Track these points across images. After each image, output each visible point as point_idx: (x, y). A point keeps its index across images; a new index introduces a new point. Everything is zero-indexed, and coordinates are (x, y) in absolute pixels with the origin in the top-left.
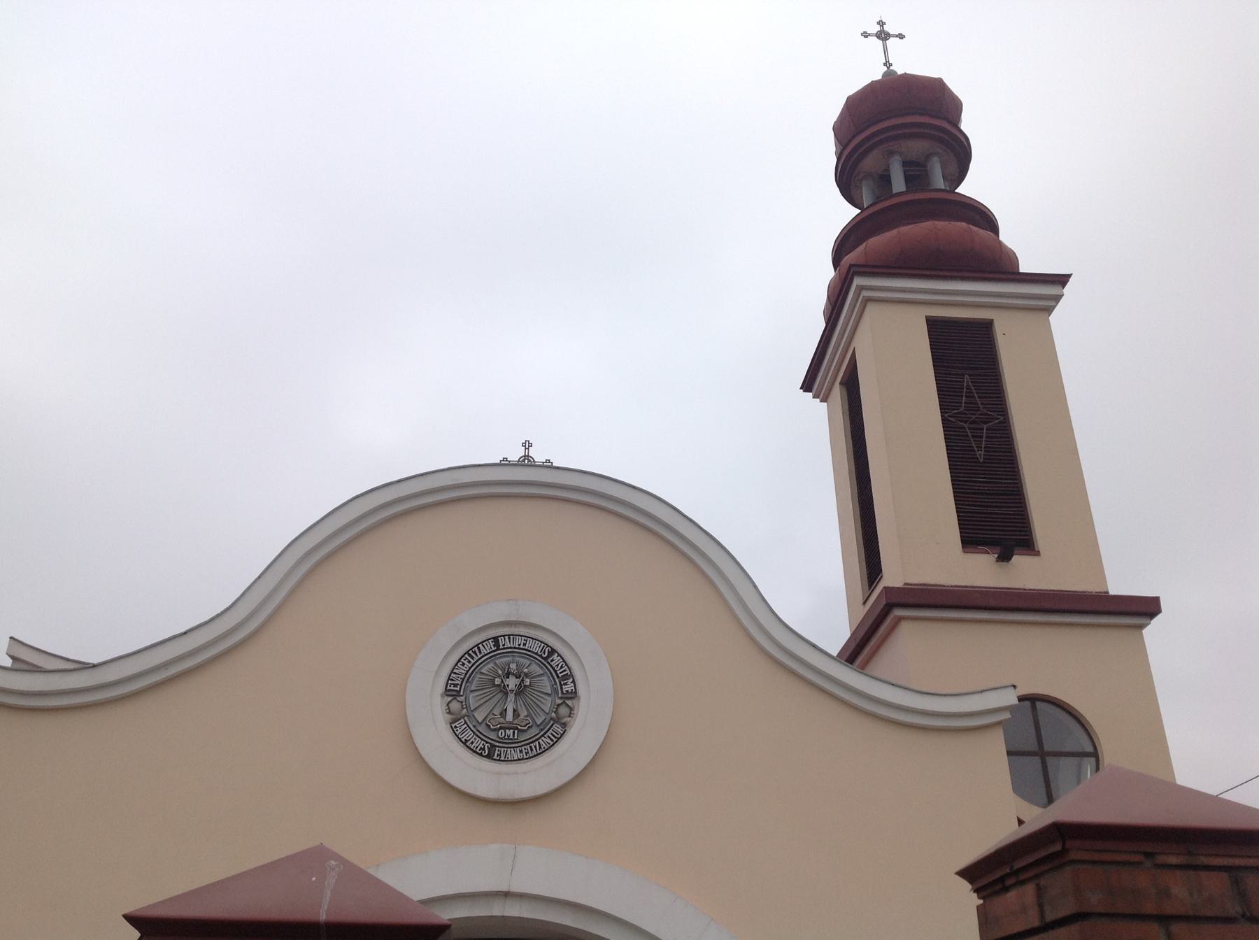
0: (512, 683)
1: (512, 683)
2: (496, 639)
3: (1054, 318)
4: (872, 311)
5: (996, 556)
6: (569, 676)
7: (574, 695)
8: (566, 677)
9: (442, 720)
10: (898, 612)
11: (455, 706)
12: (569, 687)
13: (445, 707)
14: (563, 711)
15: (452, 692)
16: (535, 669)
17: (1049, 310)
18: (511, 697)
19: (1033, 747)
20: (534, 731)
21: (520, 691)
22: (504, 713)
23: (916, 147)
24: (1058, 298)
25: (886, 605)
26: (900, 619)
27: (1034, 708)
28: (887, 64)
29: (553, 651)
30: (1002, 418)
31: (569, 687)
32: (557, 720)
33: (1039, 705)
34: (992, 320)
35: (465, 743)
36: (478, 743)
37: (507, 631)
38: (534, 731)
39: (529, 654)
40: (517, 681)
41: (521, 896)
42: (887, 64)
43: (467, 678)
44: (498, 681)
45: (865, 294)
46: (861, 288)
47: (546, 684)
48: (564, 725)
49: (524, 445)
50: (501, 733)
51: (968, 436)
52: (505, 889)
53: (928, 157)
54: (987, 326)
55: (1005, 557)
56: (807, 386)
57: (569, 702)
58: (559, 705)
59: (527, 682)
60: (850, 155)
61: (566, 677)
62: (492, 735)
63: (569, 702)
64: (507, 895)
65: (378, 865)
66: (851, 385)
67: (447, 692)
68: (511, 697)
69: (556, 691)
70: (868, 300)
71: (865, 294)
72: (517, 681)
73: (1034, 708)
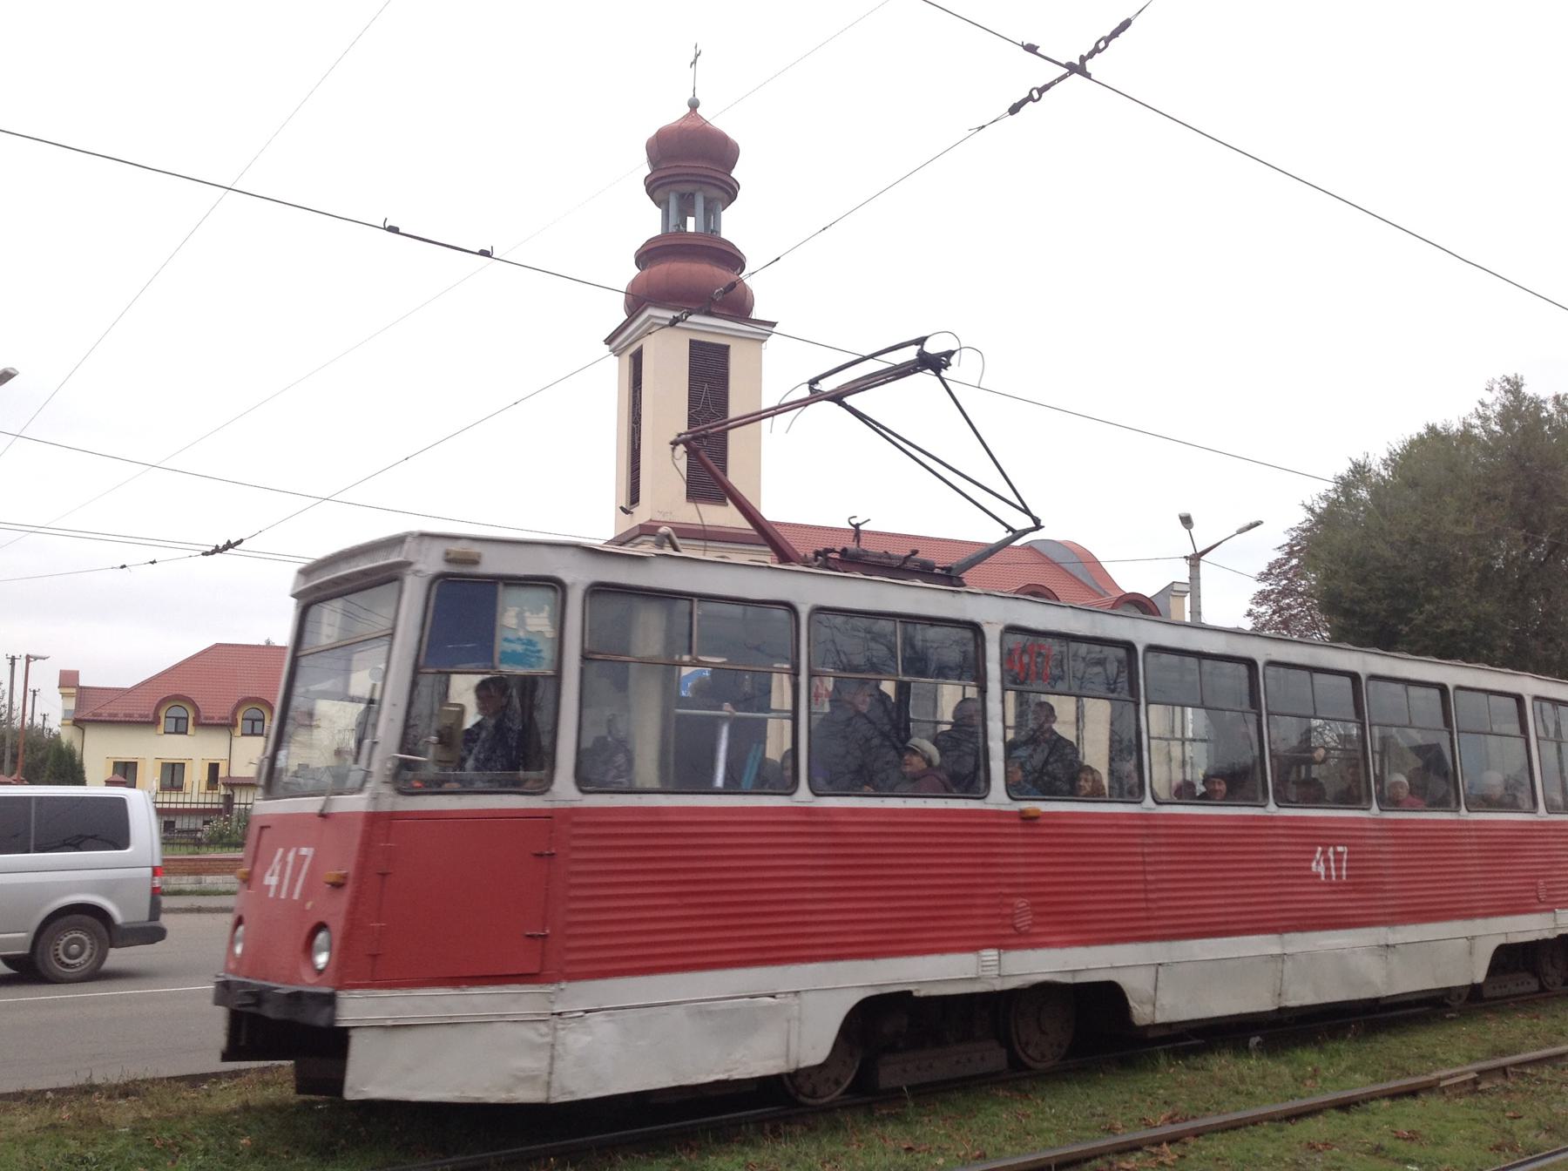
23: (688, 188)
28: (694, 105)
42: (694, 105)
54: (725, 350)
60: (655, 180)
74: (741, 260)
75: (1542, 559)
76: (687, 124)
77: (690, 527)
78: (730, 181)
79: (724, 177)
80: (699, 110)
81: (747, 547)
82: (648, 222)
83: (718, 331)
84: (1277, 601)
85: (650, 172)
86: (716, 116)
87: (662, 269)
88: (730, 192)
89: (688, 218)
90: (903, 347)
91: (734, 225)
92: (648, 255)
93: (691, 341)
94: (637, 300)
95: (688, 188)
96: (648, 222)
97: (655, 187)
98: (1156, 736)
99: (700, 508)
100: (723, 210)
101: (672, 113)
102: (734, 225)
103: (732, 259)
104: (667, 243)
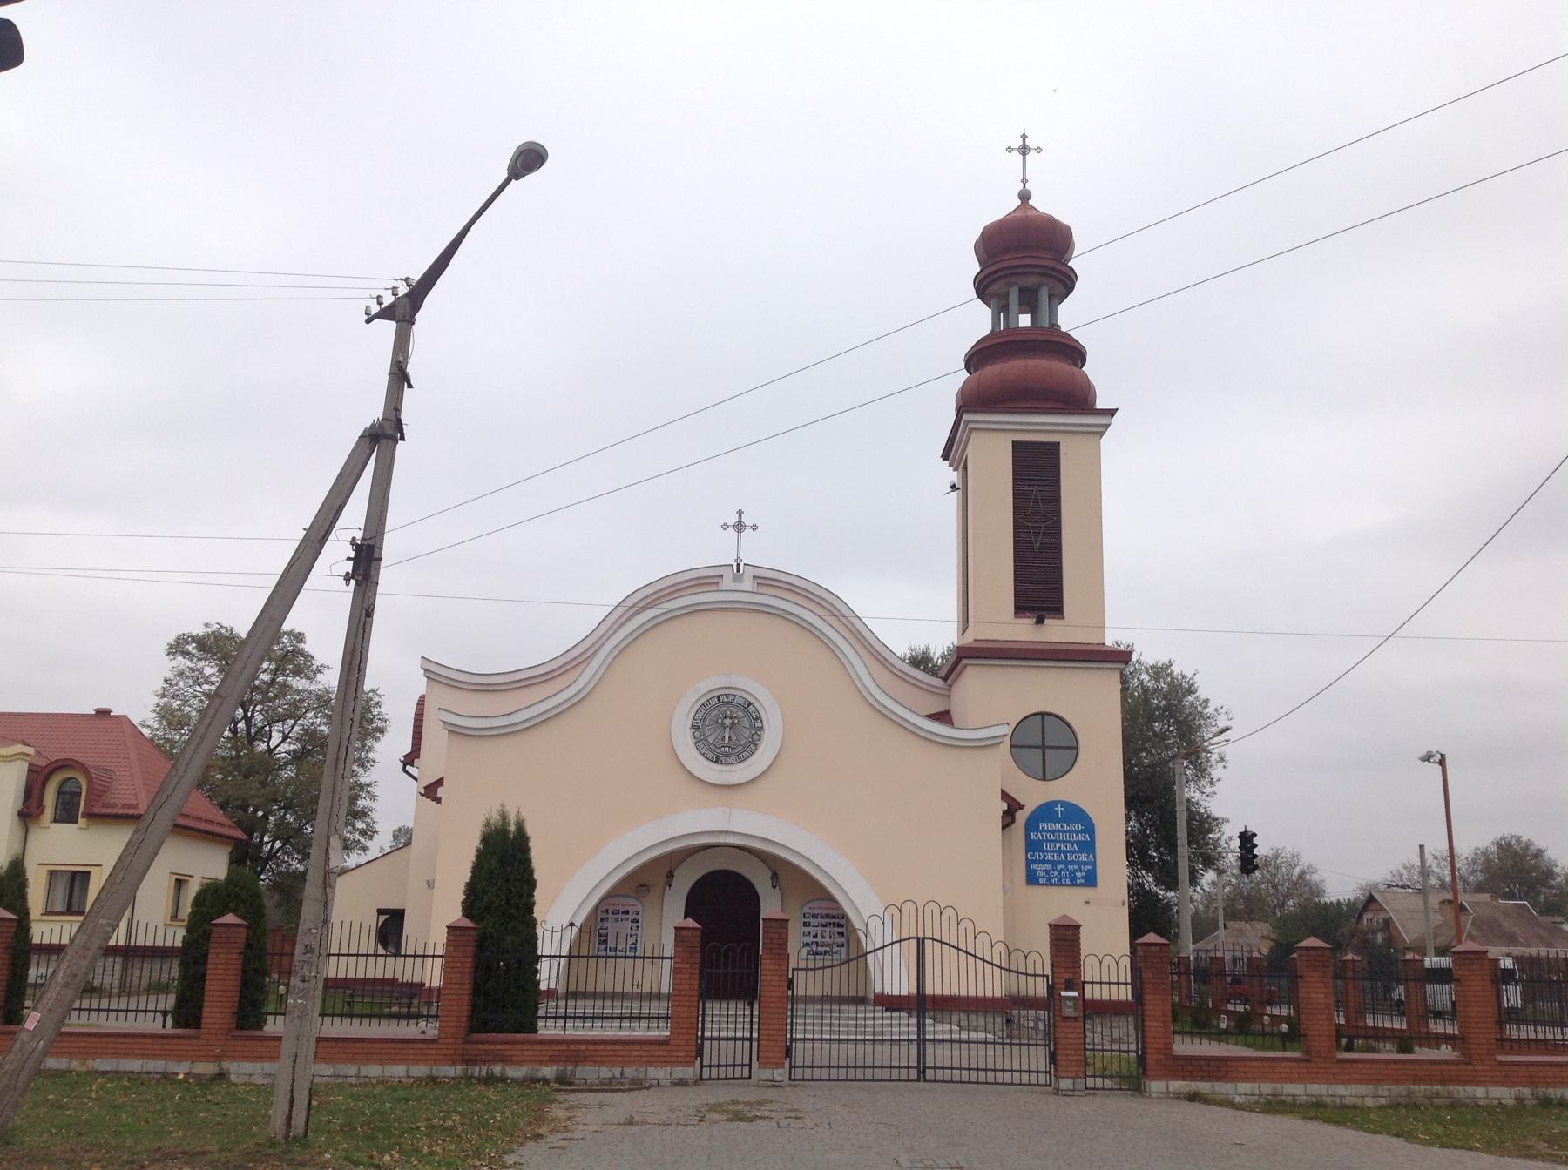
0: (728, 722)
1: (728, 722)
2: (718, 697)
3: (1105, 441)
4: (974, 436)
5: (1035, 620)
6: (759, 718)
7: (761, 729)
8: (757, 719)
9: (690, 741)
10: (965, 662)
11: (697, 734)
12: (759, 724)
13: (692, 735)
14: (756, 737)
15: (695, 727)
16: (741, 714)
17: (1101, 434)
18: (727, 729)
19: (1040, 744)
20: (740, 748)
21: (732, 726)
22: (723, 738)
23: (1030, 281)
24: (1108, 426)
25: (957, 658)
26: (966, 666)
27: (1043, 720)
28: (1025, 196)
29: (750, 704)
30: (1055, 518)
31: (759, 724)
32: (752, 742)
33: (1046, 717)
34: (1059, 443)
35: (703, 755)
36: (710, 755)
37: (728, 692)
38: (740, 748)
39: (737, 705)
40: (731, 721)
41: (734, 833)
42: (1025, 196)
43: (704, 719)
44: (720, 721)
45: (970, 426)
46: (968, 422)
47: (746, 723)
48: (756, 745)
49: (725, 529)
50: (723, 749)
51: (1030, 532)
52: (725, 830)
53: (1040, 286)
54: (1056, 446)
55: (1040, 621)
56: (945, 456)
57: (758, 732)
58: (753, 735)
59: (736, 721)
60: (987, 277)
61: (757, 719)
62: (718, 751)
63: (758, 732)
64: (726, 832)
65: (661, 817)
66: (965, 468)
67: (693, 726)
68: (727, 729)
69: (751, 726)
70: (973, 429)
71: (970, 426)
72: (731, 721)
73: (1043, 720)
74: (1081, 351)
75: (259, 869)
76: (1020, 214)
77: (1071, 647)
78: (1067, 271)
79: (1059, 267)
80: (1031, 202)
81: (1093, 665)
82: (979, 321)
83: (1031, 428)
84: (124, 991)
85: (979, 270)
86: (1043, 204)
87: (993, 371)
88: (1066, 282)
89: (1029, 315)
90: (484, 211)
91: (1070, 316)
92: (977, 358)
93: (1015, 444)
94: (971, 402)
95: (1030, 281)
96: (979, 321)
97: (983, 288)
98: (1155, 1090)
99: (307, 588)
100: (1060, 303)
101: (1003, 206)
102: (1070, 316)
103: (1074, 353)
104: (996, 341)
